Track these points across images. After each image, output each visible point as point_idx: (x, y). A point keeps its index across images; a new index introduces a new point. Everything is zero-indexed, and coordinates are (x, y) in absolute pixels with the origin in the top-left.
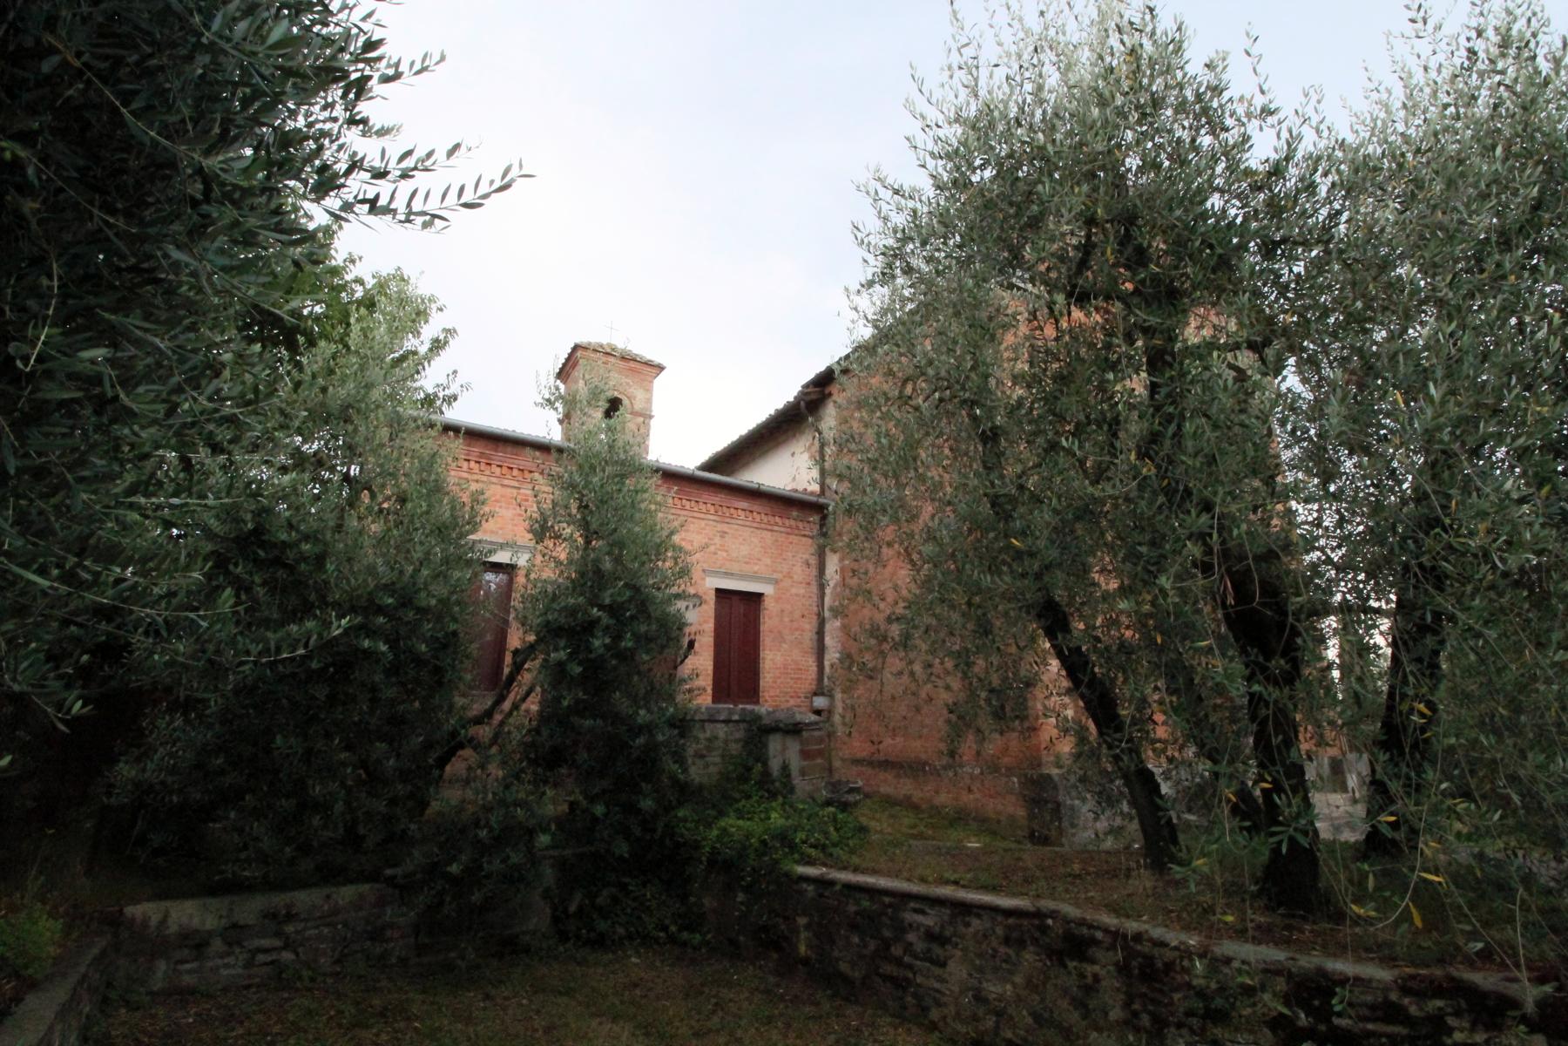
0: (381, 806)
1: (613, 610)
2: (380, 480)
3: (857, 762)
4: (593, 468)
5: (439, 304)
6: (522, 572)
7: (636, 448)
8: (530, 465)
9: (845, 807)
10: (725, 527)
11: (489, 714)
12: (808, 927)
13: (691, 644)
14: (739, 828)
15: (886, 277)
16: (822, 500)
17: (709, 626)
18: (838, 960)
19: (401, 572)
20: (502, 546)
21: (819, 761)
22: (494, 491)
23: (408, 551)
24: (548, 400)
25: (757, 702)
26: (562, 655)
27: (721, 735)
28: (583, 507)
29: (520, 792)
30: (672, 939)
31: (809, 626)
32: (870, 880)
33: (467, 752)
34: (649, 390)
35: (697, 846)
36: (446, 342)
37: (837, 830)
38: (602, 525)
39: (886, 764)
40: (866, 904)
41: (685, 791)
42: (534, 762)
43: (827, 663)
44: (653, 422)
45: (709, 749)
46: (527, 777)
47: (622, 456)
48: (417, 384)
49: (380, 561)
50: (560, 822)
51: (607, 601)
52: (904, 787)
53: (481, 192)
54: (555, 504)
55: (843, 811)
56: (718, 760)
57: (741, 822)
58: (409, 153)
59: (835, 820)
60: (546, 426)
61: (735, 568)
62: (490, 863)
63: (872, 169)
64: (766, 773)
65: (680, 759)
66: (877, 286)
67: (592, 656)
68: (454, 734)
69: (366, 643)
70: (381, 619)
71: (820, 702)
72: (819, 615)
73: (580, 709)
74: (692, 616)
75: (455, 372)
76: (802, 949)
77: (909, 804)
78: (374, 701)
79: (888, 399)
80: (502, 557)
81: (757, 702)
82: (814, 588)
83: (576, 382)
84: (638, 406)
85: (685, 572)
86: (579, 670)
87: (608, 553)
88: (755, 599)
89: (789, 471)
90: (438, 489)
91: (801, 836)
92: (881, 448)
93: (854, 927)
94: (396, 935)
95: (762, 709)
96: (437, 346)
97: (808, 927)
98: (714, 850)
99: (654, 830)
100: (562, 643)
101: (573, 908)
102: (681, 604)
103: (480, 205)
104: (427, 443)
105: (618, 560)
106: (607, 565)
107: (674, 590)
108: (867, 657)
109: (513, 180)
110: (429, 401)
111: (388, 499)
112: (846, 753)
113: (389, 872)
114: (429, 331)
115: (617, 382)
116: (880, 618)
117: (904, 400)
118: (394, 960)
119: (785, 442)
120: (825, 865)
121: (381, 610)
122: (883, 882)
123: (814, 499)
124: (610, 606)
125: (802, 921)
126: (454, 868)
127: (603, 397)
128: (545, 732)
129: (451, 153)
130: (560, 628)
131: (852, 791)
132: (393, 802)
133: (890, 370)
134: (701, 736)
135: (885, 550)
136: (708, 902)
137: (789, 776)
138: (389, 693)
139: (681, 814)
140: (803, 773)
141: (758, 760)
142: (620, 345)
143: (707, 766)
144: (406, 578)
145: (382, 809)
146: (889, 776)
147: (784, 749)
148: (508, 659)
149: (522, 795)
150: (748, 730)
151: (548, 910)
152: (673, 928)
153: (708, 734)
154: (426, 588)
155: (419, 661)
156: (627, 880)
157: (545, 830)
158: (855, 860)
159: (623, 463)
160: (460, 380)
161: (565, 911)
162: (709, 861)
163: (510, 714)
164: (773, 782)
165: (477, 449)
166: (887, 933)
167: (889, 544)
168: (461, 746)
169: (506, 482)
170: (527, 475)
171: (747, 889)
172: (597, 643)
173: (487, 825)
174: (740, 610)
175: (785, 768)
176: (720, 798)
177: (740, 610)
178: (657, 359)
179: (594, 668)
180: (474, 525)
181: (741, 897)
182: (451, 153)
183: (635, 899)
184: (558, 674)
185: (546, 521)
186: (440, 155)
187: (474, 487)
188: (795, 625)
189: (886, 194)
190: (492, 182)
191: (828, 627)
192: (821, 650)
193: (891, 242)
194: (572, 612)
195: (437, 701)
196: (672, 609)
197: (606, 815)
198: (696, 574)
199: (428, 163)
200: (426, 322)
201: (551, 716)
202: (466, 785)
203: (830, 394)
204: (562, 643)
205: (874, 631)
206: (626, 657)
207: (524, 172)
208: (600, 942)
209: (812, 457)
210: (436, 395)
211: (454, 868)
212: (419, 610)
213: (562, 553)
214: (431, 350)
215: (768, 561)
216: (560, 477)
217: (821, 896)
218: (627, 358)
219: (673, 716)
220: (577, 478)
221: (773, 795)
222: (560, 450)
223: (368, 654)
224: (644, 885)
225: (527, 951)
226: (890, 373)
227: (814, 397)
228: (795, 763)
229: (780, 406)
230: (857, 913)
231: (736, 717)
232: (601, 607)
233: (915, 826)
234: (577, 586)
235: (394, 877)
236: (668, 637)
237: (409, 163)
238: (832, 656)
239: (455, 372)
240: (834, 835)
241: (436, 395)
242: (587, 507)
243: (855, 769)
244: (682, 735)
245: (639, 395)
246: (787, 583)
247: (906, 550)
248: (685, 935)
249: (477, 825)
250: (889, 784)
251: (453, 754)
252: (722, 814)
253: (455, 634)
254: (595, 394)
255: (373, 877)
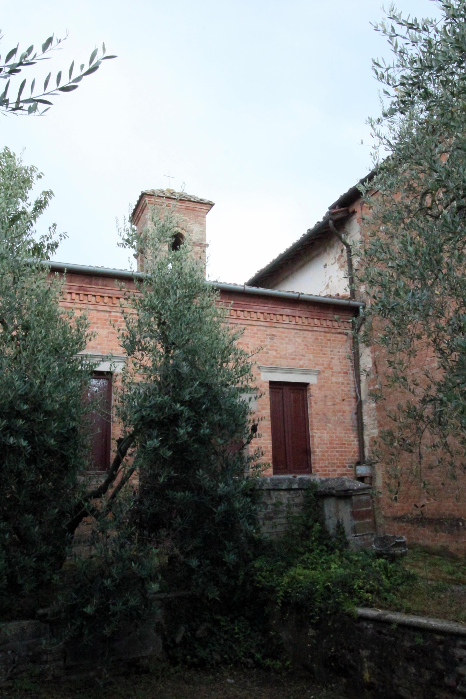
0: (31, 562)
1: (192, 404)
2: (8, 315)
3: (400, 519)
4: (167, 291)
5: (38, 173)
6: (119, 378)
7: (199, 273)
8: (117, 294)
9: (393, 558)
10: (274, 331)
11: (103, 489)
12: (370, 658)
13: (254, 429)
14: (306, 576)
15: (404, 105)
16: (353, 303)
17: (266, 412)
18: (398, 686)
19: (32, 385)
20: (103, 358)
21: (368, 520)
22: (93, 316)
23: (35, 368)
24: (127, 241)
25: (310, 472)
26: (155, 443)
27: (285, 501)
28: (161, 324)
29: (131, 549)
30: (258, 664)
31: (349, 408)
32: (422, 621)
33: (90, 519)
34: (202, 224)
35: (272, 590)
36: (46, 203)
37: (388, 578)
38: (177, 337)
39: (421, 520)
40: (419, 640)
41: (259, 547)
42: (141, 527)
43: (367, 439)
44: (208, 250)
45: (276, 512)
46: (135, 538)
47: (189, 281)
48: (29, 238)
49: (16, 377)
50: (162, 570)
51: (187, 398)
52: (441, 540)
53: (74, 76)
54: (140, 324)
55: (392, 562)
56: (284, 521)
57: (307, 572)
58: (13, 52)
59: (386, 568)
60: (124, 261)
61: (284, 363)
62: (114, 604)
63: (387, 9)
64: (324, 531)
65: (253, 520)
66: (398, 114)
67: (179, 442)
68: (79, 506)
69: (12, 440)
70: (21, 422)
71: (363, 470)
72: (356, 398)
73: (172, 484)
74: (253, 406)
75: (55, 225)
76: (367, 676)
77: (444, 553)
78: (20, 483)
79: (410, 211)
80: (104, 367)
81: (310, 472)
82: (351, 377)
83: (146, 223)
84: (195, 237)
85: (245, 371)
86: (170, 453)
87: (184, 360)
88: (302, 387)
89: (324, 279)
90: (51, 317)
91: (358, 583)
92: (409, 254)
93: (410, 659)
94: (50, 658)
95: (317, 478)
96: (40, 206)
97: (370, 658)
98: (287, 595)
99: (237, 578)
100: (155, 433)
101: (178, 639)
102: (245, 397)
103: (75, 87)
104: (41, 283)
105: (192, 364)
106: (185, 369)
107: (239, 385)
108: (407, 433)
109: (99, 63)
110: (37, 249)
111: (16, 328)
112: (388, 512)
113: (41, 611)
114: (34, 195)
115: (180, 220)
116: (415, 400)
117: (424, 210)
118: (50, 678)
119: (318, 255)
120: (381, 607)
121: (19, 415)
122: (433, 623)
123: (346, 302)
124: (190, 401)
125: (365, 653)
126: (89, 610)
127: (169, 233)
128: (147, 502)
129: (45, 47)
130: (152, 421)
131: (398, 545)
132: (40, 558)
133: (410, 186)
134: (269, 502)
135: (416, 342)
136: (285, 636)
137: (343, 533)
138: (30, 477)
139: (257, 565)
140: (355, 530)
141: (316, 521)
142: (177, 189)
143: (274, 526)
144: (35, 389)
145: (33, 565)
146: (427, 531)
147: (338, 511)
148: (114, 446)
149: (134, 553)
150: (306, 497)
151: (160, 641)
152: (258, 656)
153: (274, 501)
154: (50, 395)
155: (50, 452)
156: (219, 617)
157: (153, 579)
158: (406, 603)
159: (189, 286)
160: (59, 230)
161: (173, 641)
162: (283, 602)
163: (119, 488)
164: (330, 538)
165: (76, 284)
166: (440, 666)
167: (419, 337)
168: (86, 515)
169: (100, 308)
170: (115, 301)
171: (316, 626)
172: (182, 432)
173: (110, 576)
174: (290, 398)
175: (339, 526)
176: (290, 550)
177: (290, 398)
178: (207, 198)
179: (181, 450)
180: (80, 342)
181: (311, 632)
182: (45, 47)
183: (226, 632)
184: (155, 458)
185: (134, 337)
186: (38, 49)
187: (77, 314)
188: (337, 407)
189: (402, 30)
190: (82, 66)
191: (365, 407)
192: (360, 427)
193: (408, 72)
194: (160, 408)
195: (65, 482)
196: (238, 401)
197: (199, 566)
198: (254, 370)
199: (29, 58)
200: (30, 188)
201: (149, 490)
202: (90, 545)
203: (354, 212)
204: (155, 433)
205: (414, 415)
206: (204, 441)
207: (107, 54)
208: (201, 665)
209: (342, 266)
210: (42, 244)
211: (89, 610)
212: (48, 413)
213: (147, 361)
214: (35, 209)
215: (311, 357)
216: (142, 301)
217: (380, 632)
218: (184, 200)
219: (246, 487)
220: (156, 302)
221: (331, 549)
222: (140, 280)
223: (15, 449)
224: (232, 621)
225: (147, 671)
226: (411, 188)
227: (340, 216)
228: (348, 523)
229: (312, 226)
230: (412, 648)
231: (295, 486)
232: (183, 403)
233: (452, 573)
234: (162, 387)
235: (46, 615)
236: (235, 423)
237: (15, 59)
238: (371, 431)
239: (55, 225)
240: (386, 582)
241: (42, 244)
242: (164, 323)
243: (396, 526)
244: (253, 502)
245: (196, 228)
246: (328, 373)
247: (434, 341)
248: (268, 662)
249: (102, 575)
250: (427, 537)
251: (80, 521)
252: (290, 565)
253: (74, 429)
254: (163, 231)
255: (31, 615)
